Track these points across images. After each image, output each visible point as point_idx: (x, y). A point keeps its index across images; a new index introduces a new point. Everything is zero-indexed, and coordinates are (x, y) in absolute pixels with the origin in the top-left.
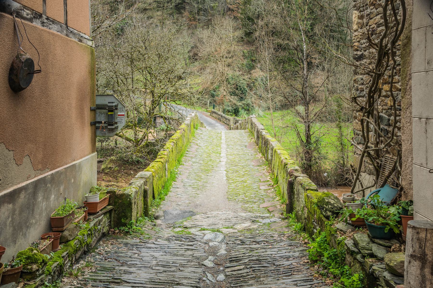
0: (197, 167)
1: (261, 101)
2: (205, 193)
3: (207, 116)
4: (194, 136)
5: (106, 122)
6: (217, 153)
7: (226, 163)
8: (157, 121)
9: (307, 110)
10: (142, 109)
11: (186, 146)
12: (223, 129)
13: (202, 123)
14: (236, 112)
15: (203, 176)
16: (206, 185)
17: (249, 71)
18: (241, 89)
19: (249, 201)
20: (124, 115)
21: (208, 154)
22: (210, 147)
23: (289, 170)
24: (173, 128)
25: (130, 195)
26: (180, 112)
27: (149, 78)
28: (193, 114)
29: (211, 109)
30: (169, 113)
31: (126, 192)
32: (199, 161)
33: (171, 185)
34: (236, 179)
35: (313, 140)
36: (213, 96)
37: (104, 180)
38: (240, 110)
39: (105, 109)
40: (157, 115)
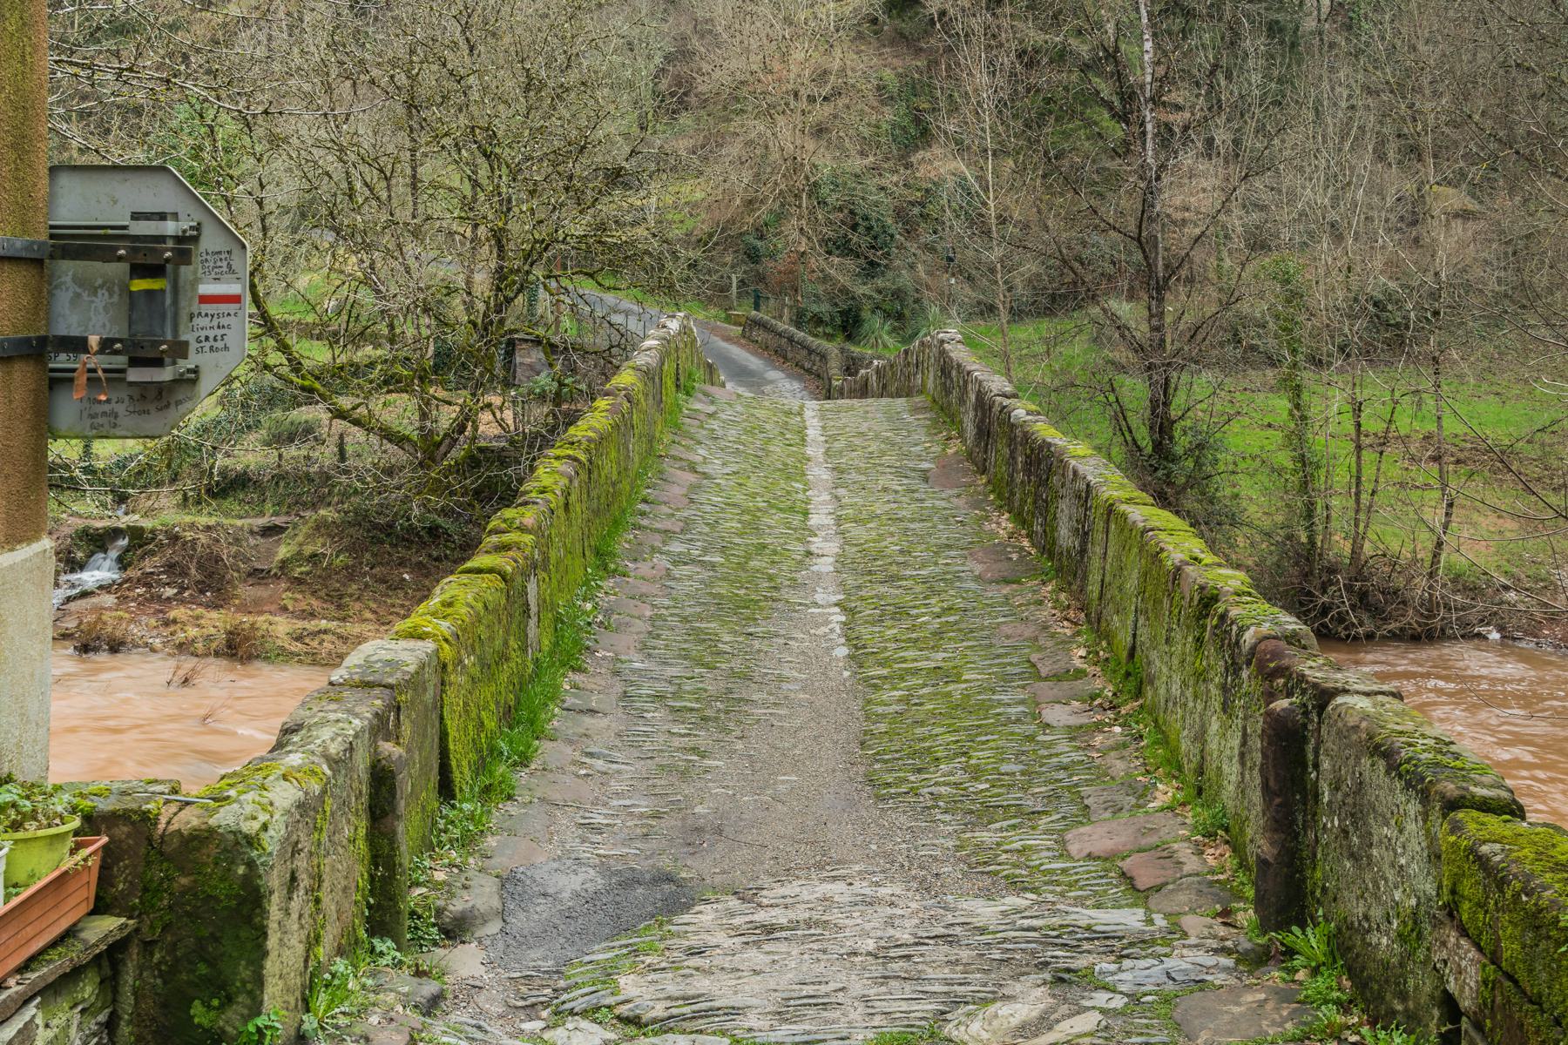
1: (953, 281)
2: (739, 746)
3: (728, 339)
4: (678, 426)
5: (113, 341)
6: (792, 509)
7: (841, 560)
8: (518, 360)
9: (1156, 316)
10: (456, 309)
11: (638, 476)
12: (799, 395)
13: (710, 366)
14: (849, 324)
15: (727, 638)
16: (744, 695)
17: (902, 157)
18: (869, 229)
19: (993, 801)
20: (236, 299)
21: (747, 517)
22: (753, 478)
23: (1249, 637)
24: (583, 387)
25: (251, 841)
26: (617, 319)
27: (483, 172)
28: (674, 325)
29: (745, 310)
30: (566, 322)
31: (224, 818)
32: (705, 551)
33: (552, 699)
34: (905, 661)
35: (1181, 443)
36: (753, 256)
37: (284, 609)
38: (866, 314)
39: (108, 255)
40: (517, 331)
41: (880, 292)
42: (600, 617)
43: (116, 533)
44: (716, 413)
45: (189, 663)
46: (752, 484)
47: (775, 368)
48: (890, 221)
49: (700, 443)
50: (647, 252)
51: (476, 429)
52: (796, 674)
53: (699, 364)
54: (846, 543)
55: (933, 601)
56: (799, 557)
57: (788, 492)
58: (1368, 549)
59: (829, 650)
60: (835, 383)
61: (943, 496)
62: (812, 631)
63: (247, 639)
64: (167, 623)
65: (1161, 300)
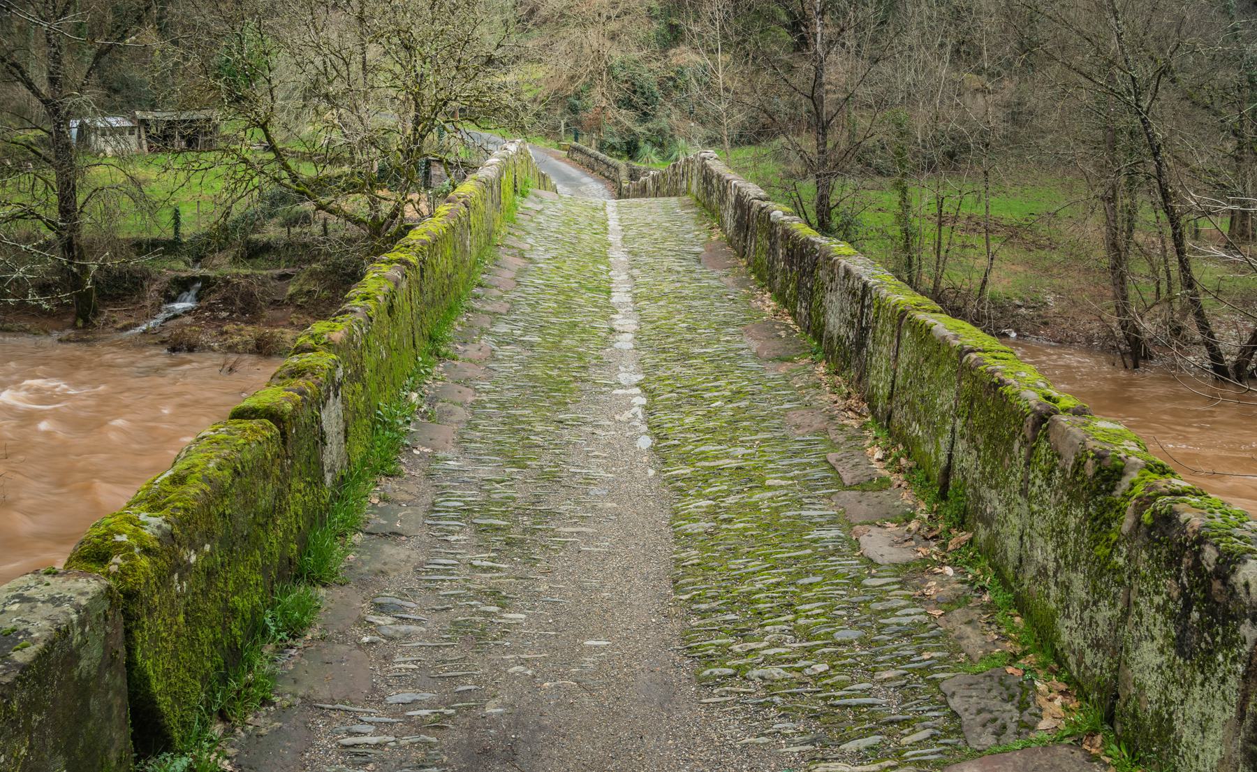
0: (516, 366)
3: (559, 159)
6: (598, 289)
7: (639, 336)
8: (433, 172)
13: (544, 176)
14: (631, 150)
15: (539, 428)
18: (643, 93)
21: (562, 297)
22: (568, 262)
28: (512, 148)
29: (569, 141)
36: (574, 110)
38: (641, 144)
41: (650, 131)
42: (425, 407)
43: (194, 280)
44: (543, 210)
45: (233, 358)
46: (567, 268)
47: (588, 176)
48: (655, 89)
49: (529, 233)
50: (508, 107)
51: (403, 215)
52: (603, 473)
53: (534, 175)
54: (643, 320)
55: (722, 383)
56: (604, 334)
57: (595, 274)
58: (943, 284)
59: (634, 439)
60: (624, 185)
61: (715, 276)
62: (617, 417)
63: (268, 343)
64: (222, 333)
65: (825, 135)
